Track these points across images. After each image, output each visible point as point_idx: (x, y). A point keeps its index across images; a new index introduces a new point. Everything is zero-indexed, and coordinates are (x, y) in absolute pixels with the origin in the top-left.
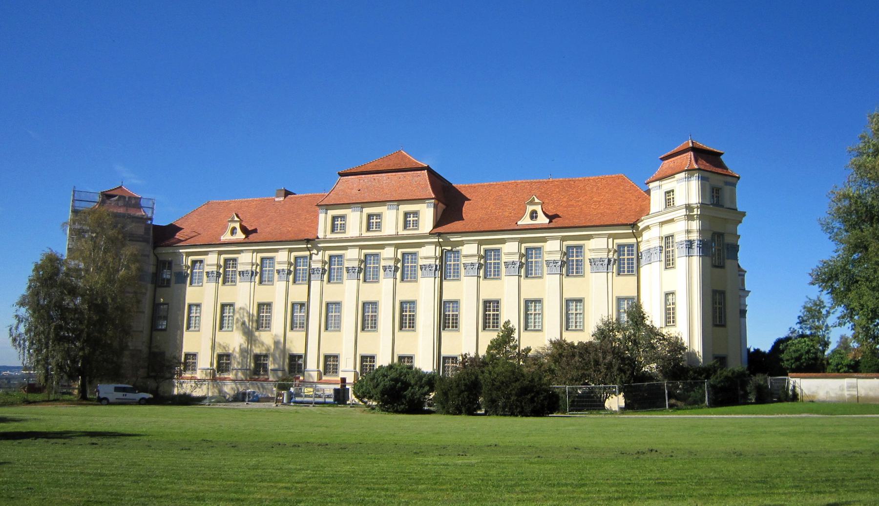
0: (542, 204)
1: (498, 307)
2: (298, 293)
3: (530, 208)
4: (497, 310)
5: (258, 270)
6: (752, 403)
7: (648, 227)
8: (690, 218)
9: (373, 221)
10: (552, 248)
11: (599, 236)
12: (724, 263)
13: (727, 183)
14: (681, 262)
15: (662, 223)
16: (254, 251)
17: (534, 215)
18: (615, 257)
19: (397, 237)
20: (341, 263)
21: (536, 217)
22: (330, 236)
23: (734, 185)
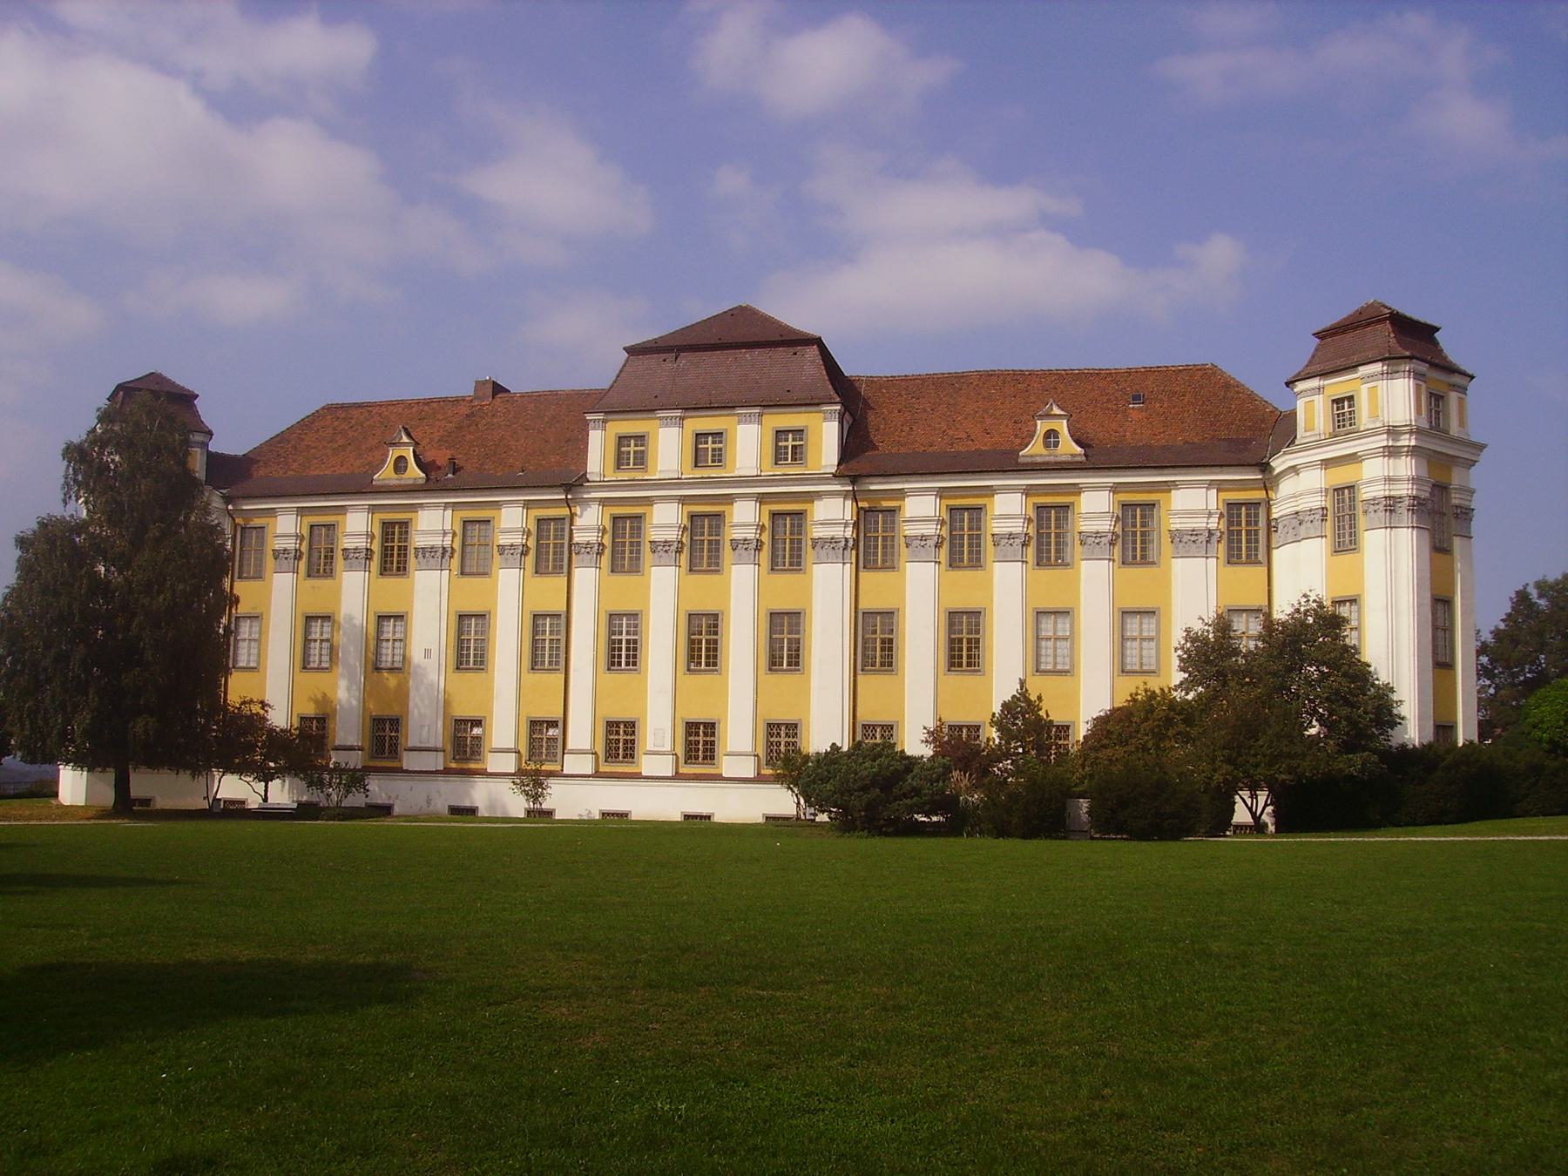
0: (1069, 417)
1: (716, 626)
2: (548, 593)
3: (1042, 426)
4: (635, 633)
5: (457, 546)
6: (1080, 833)
7: (1294, 470)
8: (1391, 452)
9: (707, 450)
10: (1095, 505)
11: (436, 505)
12: (1451, 544)
13: (1454, 387)
14: (1374, 540)
15: (1327, 463)
16: (1211, 484)
17: (400, 464)
18: (1223, 526)
19: (677, 483)
20: (976, 524)
21: (1056, 444)
22: (611, 476)
23: (1463, 390)
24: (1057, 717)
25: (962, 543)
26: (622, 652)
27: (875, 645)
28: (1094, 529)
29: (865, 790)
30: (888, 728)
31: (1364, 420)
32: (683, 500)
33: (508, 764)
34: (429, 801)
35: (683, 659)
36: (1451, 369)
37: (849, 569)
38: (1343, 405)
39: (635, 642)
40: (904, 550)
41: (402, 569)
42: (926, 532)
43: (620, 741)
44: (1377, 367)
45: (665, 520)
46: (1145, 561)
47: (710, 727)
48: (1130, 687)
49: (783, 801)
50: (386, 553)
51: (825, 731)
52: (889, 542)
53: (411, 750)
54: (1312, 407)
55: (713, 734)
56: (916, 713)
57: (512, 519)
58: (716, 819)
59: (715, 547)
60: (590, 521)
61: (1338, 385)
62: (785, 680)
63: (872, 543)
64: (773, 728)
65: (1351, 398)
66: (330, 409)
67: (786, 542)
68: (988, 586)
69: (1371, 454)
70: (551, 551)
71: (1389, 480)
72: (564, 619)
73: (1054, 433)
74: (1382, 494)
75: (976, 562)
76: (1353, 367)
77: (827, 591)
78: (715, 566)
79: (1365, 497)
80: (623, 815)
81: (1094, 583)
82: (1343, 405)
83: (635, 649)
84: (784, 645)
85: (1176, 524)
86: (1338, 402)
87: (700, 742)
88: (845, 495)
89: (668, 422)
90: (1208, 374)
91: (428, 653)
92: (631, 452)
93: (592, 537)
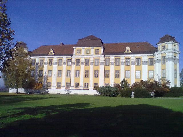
9: (87, 52)
17: (51, 53)
24: (129, 83)
25: (117, 63)
26: (77, 75)
27: (107, 75)
29: (106, 91)
31: (166, 48)
33: (64, 88)
34: (162, 91)
37: (104, 65)
38: (164, 47)
40: (110, 64)
41: (52, 65)
43: (77, 85)
47: (88, 84)
48: (138, 80)
49: (96, 92)
50: (50, 63)
51: (101, 84)
52: (109, 63)
54: (160, 47)
56: (112, 82)
59: (88, 63)
60: (74, 59)
63: (107, 63)
64: (95, 84)
65: (164, 46)
66: (42, 46)
68: (120, 68)
75: (119, 65)
77: (101, 69)
78: (88, 65)
80: (87, 94)
81: (133, 67)
82: (164, 47)
84: (96, 74)
87: (86, 86)
91: (54, 75)
92: (79, 52)
93: (74, 62)
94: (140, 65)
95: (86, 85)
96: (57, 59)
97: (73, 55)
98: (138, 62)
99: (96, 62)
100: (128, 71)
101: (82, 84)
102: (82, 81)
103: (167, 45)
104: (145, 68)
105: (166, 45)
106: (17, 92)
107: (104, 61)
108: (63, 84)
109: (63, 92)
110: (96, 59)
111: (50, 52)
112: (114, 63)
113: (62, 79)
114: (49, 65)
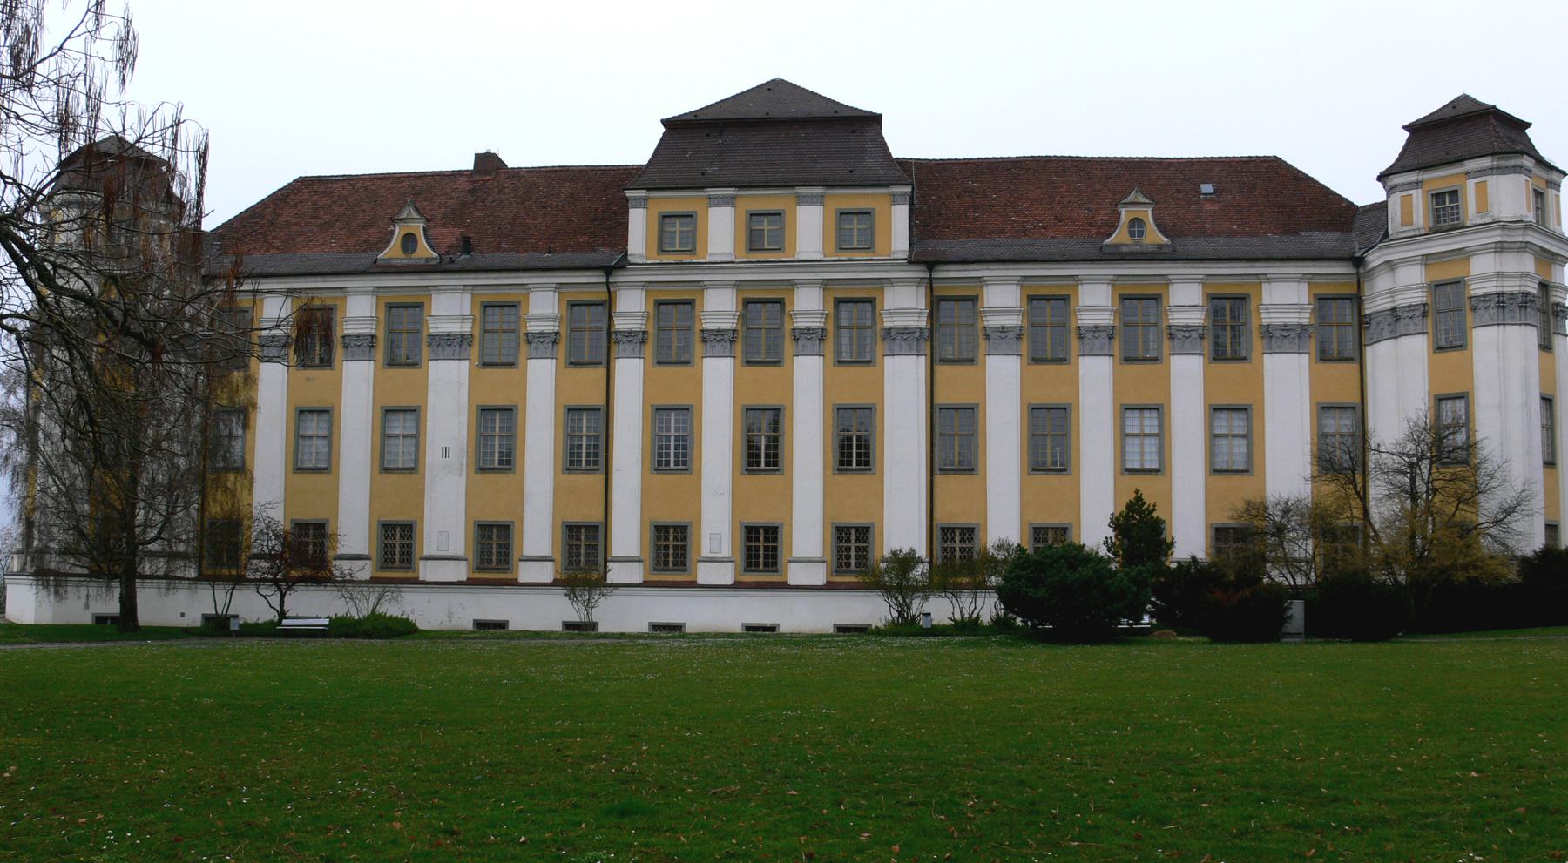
9: (762, 234)
10: (1186, 298)
11: (453, 289)
15: (1426, 260)
17: (409, 241)
21: (1141, 234)
23: (1557, 186)
25: (1048, 337)
26: (763, 450)
27: (953, 441)
28: (999, 324)
30: (1065, 530)
31: (1471, 213)
32: (738, 284)
35: (833, 459)
36: (1549, 167)
39: (685, 439)
40: (1074, 343)
42: (1007, 323)
43: (671, 549)
44: (1486, 162)
45: (720, 307)
46: (1238, 358)
47: (772, 532)
53: (428, 558)
55: (685, 538)
57: (543, 305)
58: (783, 629)
61: (1441, 178)
62: (854, 482)
63: (948, 336)
67: (854, 330)
68: (1074, 381)
69: (1482, 250)
70: (591, 342)
71: (1500, 276)
72: (604, 413)
73: (1138, 217)
74: (1494, 290)
76: (1459, 161)
79: (1473, 293)
83: (685, 448)
84: (854, 450)
85: (1267, 318)
86: (1438, 197)
87: (761, 549)
88: (919, 282)
89: (809, 200)
90: (1276, 159)
91: (446, 452)
93: (636, 325)
94: (1243, 354)
95: (853, 545)
96: (467, 297)
97: (623, 264)
98: (1229, 334)
99: (854, 330)
100: (1142, 411)
101: (716, 534)
102: (716, 507)
103: (1481, 190)
104: (1287, 386)
105: (1471, 185)
106: (583, 628)
107: (923, 323)
108: (538, 536)
109: (538, 611)
110: (854, 303)
111: (398, 232)
112: (1019, 337)
113: (375, 495)
114: (1218, 355)
